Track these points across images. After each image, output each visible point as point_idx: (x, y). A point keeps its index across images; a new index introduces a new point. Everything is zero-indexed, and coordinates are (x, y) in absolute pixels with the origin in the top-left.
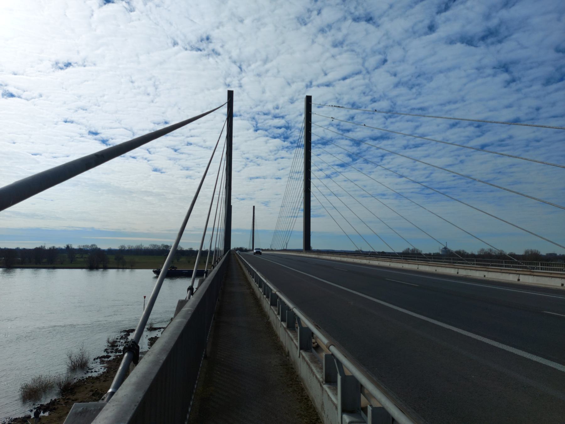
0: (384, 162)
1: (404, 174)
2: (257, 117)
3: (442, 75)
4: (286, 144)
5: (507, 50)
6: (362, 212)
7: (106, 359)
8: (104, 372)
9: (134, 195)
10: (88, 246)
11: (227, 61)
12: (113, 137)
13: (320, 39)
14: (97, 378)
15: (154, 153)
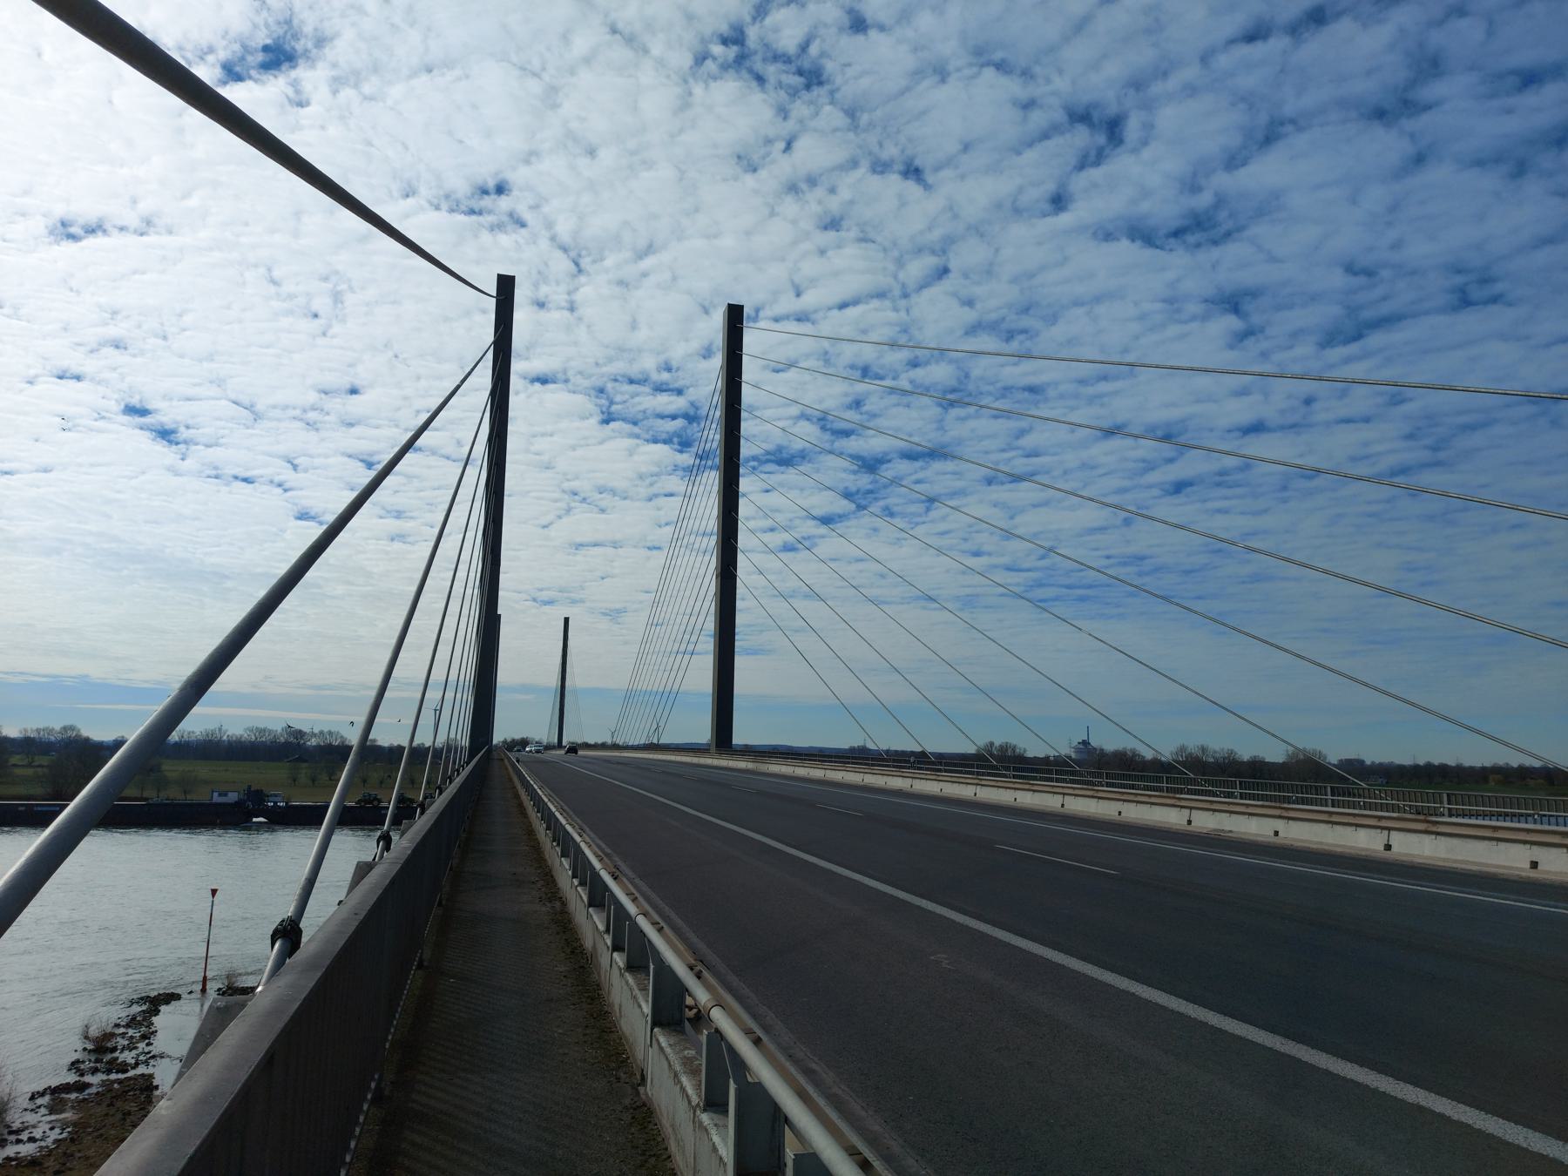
0: (933, 514)
1: (986, 548)
2: (610, 386)
3: (1080, 311)
4: (687, 459)
5: (1234, 263)
6: (879, 643)
7: (73, 1096)
8: (56, 1141)
9: (229, 584)
11: (544, 244)
12: (190, 422)
13: (790, 207)
14: (34, 1163)
15: (306, 471)
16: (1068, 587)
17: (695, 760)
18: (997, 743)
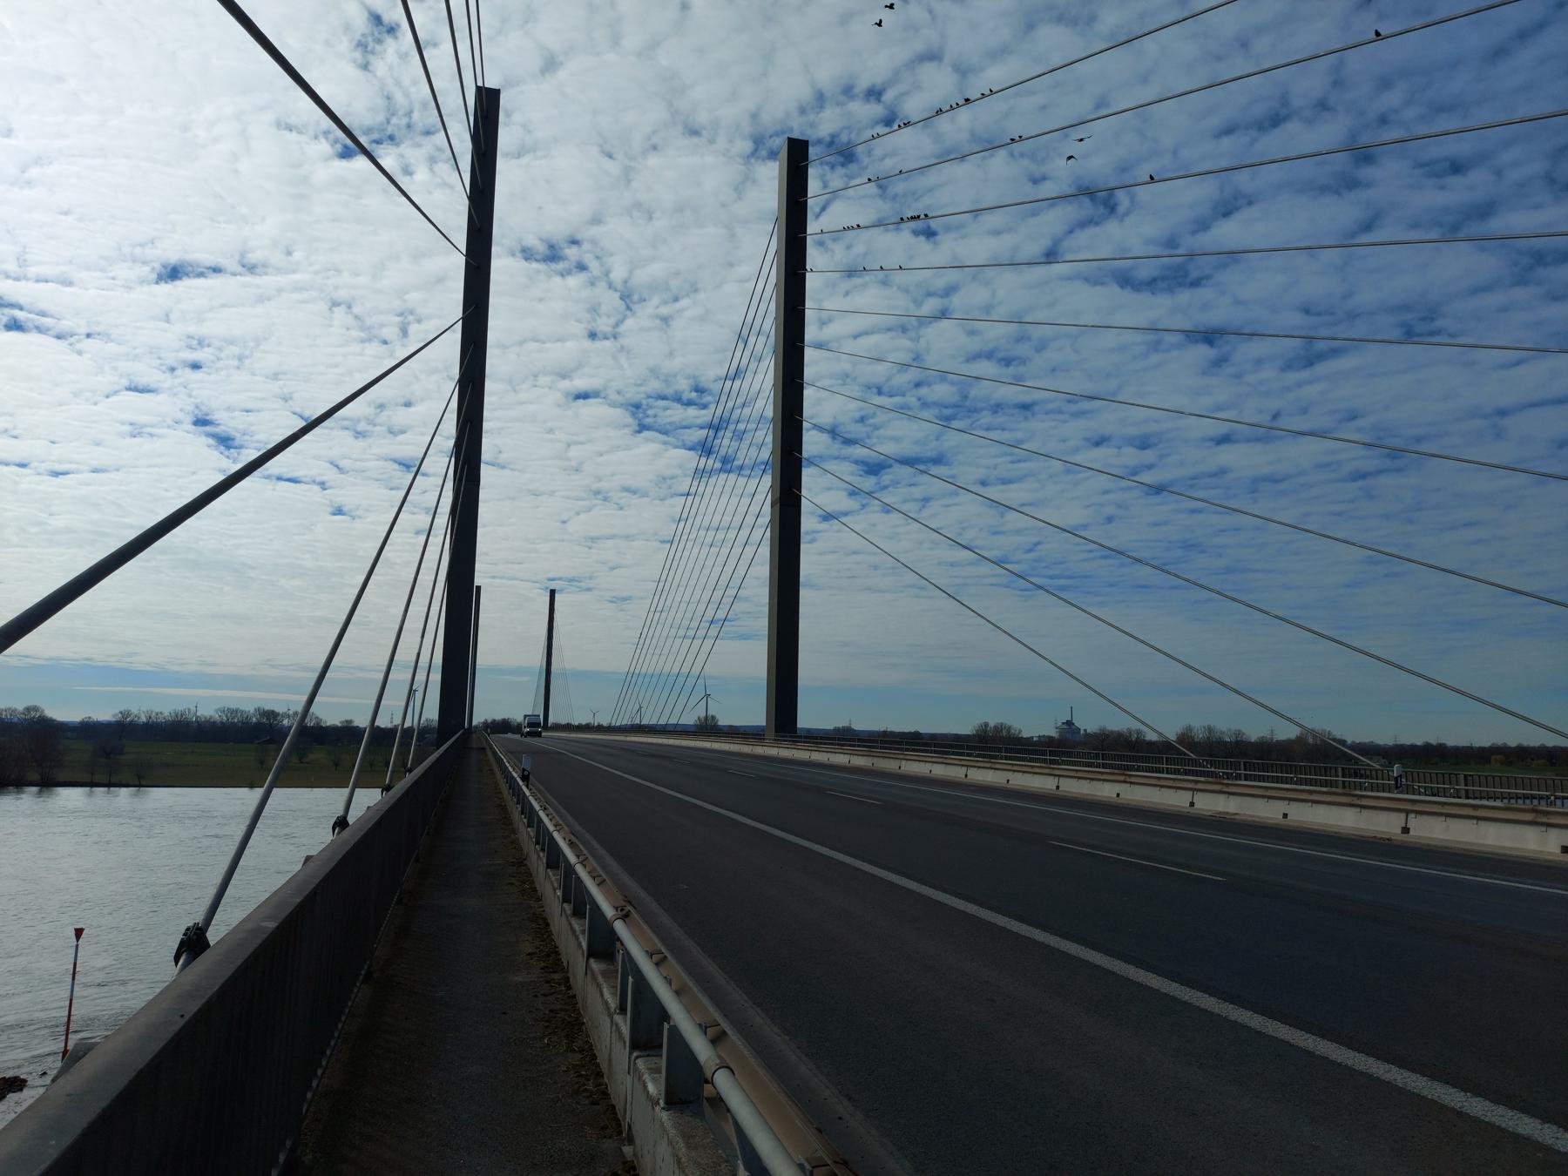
16: (1052, 577)
17: (746, 749)
18: (992, 724)
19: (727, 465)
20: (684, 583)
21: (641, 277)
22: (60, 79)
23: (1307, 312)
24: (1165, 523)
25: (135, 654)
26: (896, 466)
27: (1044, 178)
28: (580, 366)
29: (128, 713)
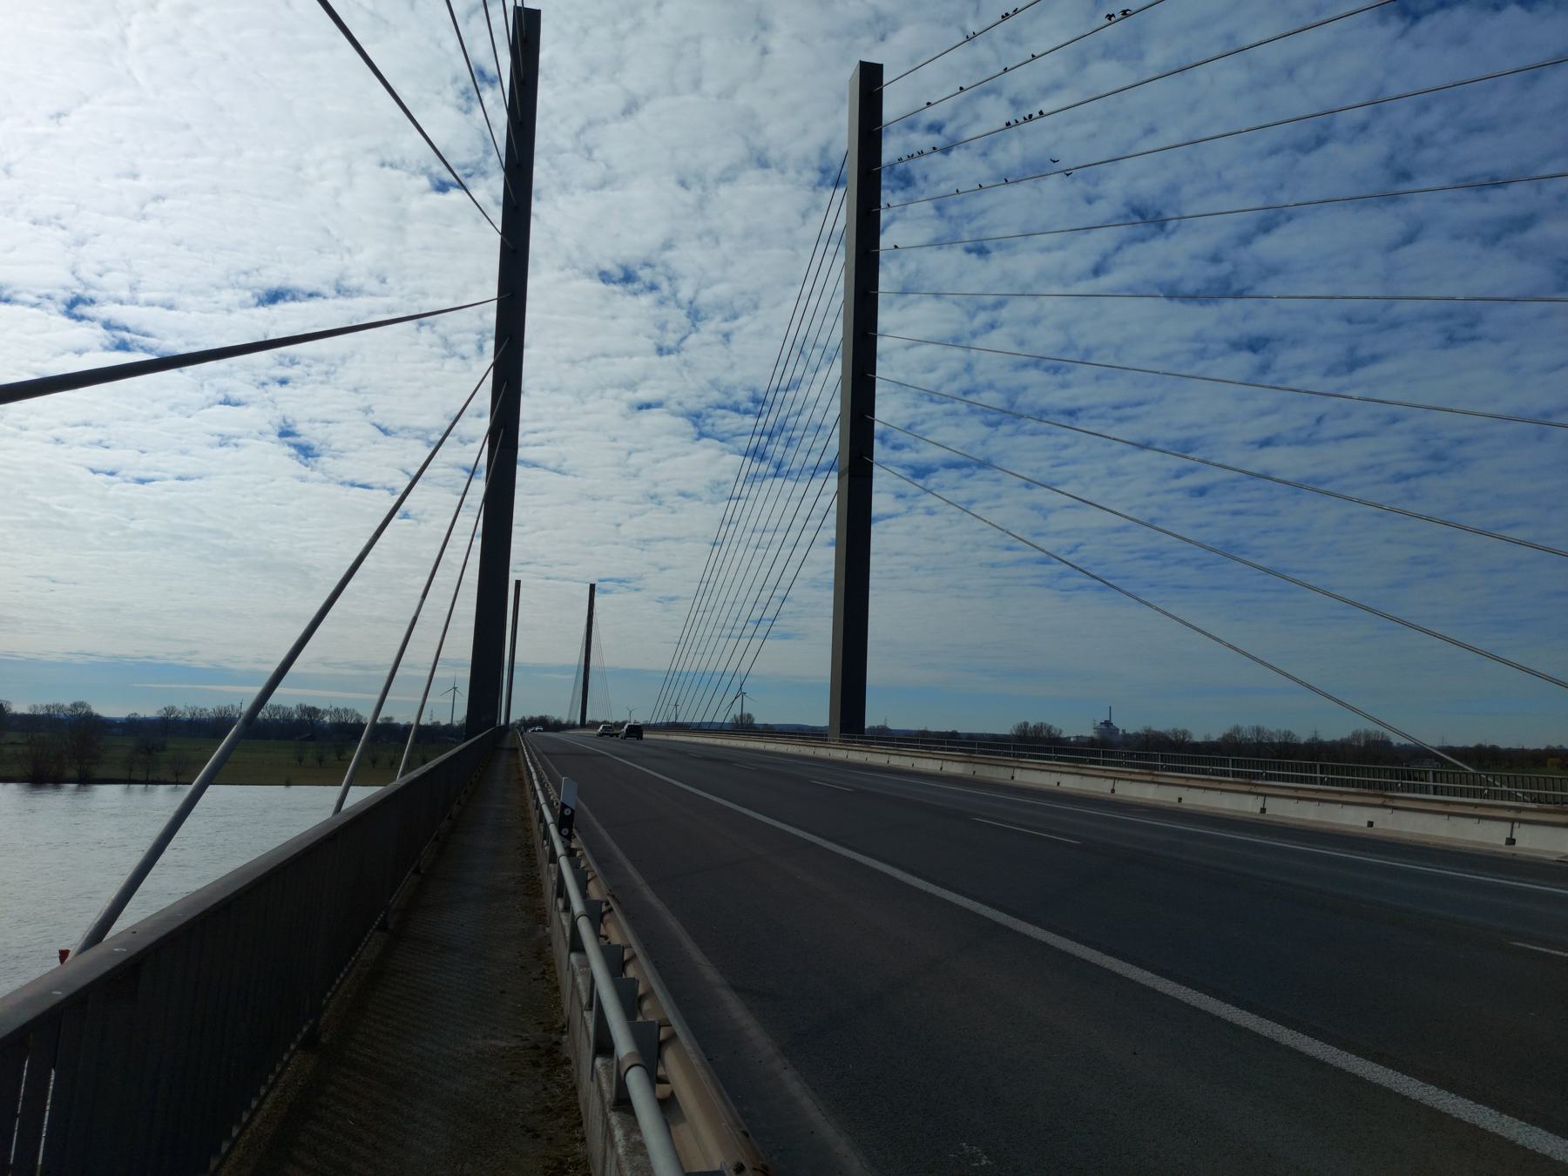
10: (61, 708)
17: (808, 751)
18: (1032, 724)
19: (779, 470)
20: (728, 583)
21: (706, 297)
22: (187, 127)
23: (1350, 321)
24: (1207, 525)
25: (196, 652)
26: (942, 470)
27: (1099, 197)
28: (645, 378)
29: (173, 710)
